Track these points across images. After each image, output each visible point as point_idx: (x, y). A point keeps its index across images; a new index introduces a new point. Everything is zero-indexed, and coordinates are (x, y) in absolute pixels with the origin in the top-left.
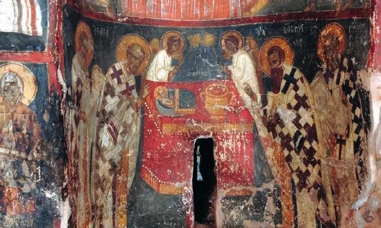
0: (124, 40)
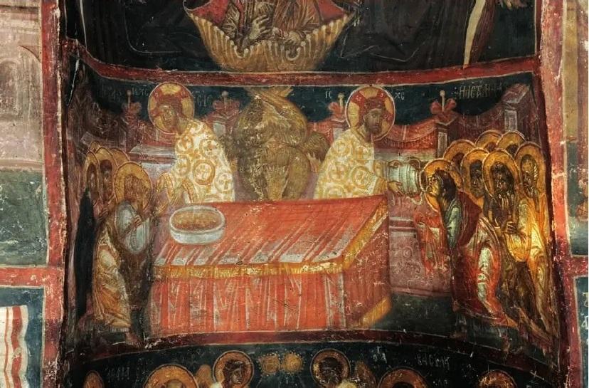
0: (154, 378)
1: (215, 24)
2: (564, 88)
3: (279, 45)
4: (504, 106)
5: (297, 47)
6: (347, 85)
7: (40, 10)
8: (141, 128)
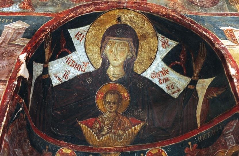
1: (89, 127)
3: (115, 136)
4: (225, 135)
6: (144, 149)
7: (8, 81)
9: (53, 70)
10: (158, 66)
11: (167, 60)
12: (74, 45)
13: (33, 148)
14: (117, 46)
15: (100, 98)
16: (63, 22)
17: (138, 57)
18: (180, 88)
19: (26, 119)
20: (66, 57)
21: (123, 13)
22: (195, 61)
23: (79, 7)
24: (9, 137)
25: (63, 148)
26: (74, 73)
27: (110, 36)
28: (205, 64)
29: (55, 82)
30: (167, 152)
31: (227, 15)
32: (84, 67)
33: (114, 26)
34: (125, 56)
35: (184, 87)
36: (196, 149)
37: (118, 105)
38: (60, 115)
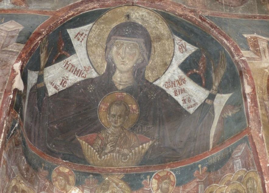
2: (264, 139)
3: (119, 155)
5: (128, 155)
6: (151, 171)
7: (3, 95)
8: (47, 184)
9: (49, 77)
10: (174, 74)
11: (185, 67)
12: (73, 47)
13: (29, 165)
14: (126, 48)
15: (103, 109)
16: (61, 22)
17: (150, 63)
18: (197, 101)
19: (21, 135)
20: (64, 61)
21: (133, 10)
22: (215, 72)
23: (80, 3)
24: (6, 153)
25: (61, 167)
26: (73, 79)
27: (117, 36)
28: (225, 78)
29: (51, 91)
30: (176, 175)
31: (255, 18)
32: (85, 72)
33: (121, 24)
34: (135, 60)
35: (201, 101)
36: (205, 173)
37: (124, 119)
38: (57, 129)
